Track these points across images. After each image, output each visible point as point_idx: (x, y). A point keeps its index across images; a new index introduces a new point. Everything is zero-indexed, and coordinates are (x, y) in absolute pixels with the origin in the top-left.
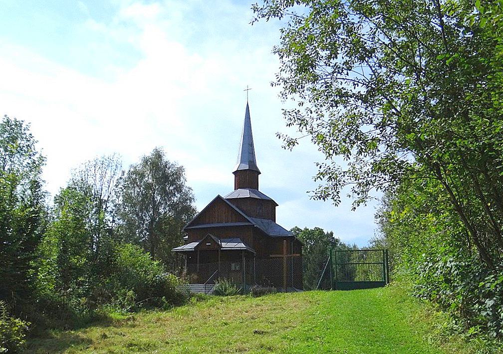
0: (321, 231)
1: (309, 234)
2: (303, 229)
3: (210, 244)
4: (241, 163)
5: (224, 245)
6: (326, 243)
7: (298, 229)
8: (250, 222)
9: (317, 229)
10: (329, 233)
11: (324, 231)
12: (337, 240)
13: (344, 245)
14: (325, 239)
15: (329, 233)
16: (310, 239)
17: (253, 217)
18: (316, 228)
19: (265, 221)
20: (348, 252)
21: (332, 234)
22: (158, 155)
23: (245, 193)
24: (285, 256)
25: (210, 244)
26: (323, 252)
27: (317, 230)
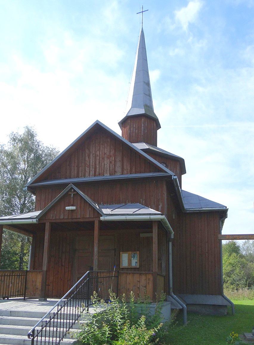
3: (74, 208)
22: (30, 135)
25: (74, 208)
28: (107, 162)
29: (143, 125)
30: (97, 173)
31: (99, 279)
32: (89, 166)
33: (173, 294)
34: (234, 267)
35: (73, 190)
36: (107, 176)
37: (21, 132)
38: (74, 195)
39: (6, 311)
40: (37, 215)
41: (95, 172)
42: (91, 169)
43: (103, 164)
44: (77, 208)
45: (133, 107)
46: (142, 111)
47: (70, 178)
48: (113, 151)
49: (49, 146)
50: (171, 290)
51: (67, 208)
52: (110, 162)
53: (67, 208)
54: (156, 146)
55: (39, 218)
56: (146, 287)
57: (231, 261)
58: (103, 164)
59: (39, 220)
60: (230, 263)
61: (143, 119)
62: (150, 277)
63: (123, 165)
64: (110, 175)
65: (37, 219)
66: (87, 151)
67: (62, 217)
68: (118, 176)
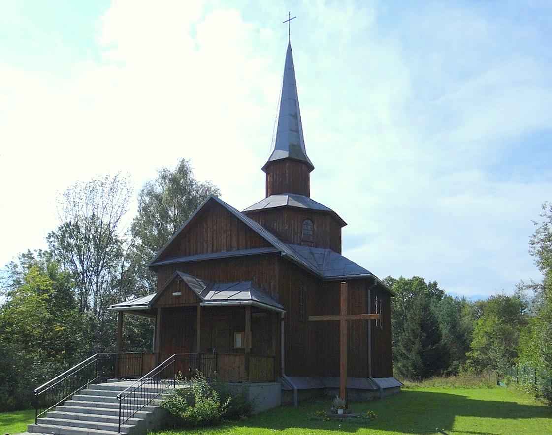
0: (421, 282)
1: (406, 285)
2: (398, 279)
3: (179, 294)
4: (275, 149)
5: (247, 295)
6: (429, 296)
7: (392, 280)
8: (270, 245)
9: (416, 278)
10: (432, 282)
11: (425, 281)
12: (442, 292)
13: (450, 298)
14: (426, 291)
15: (432, 282)
16: (407, 290)
17: (294, 244)
18: (415, 277)
19: (318, 251)
20: (457, 307)
21: (435, 284)
22: (183, 171)
23: (281, 201)
24: (343, 318)
25: (179, 294)
26: (426, 308)
27: (417, 280)
28: (223, 236)
29: (287, 171)
30: (215, 249)
31: (203, 360)
32: (207, 242)
33: (284, 375)
34: (492, 338)
35: (179, 277)
36: (224, 254)
37: (173, 169)
38: (179, 281)
39: (117, 387)
40: (150, 300)
41: (212, 249)
42: (209, 244)
43: (220, 239)
44: (182, 294)
45: (277, 147)
46: (284, 154)
47: (197, 253)
48: (230, 225)
49: (205, 184)
50: (283, 370)
51: (174, 294)
52: (227, 237)
53: (174, 294)
54: (307, 193)
55: (153, 303)
56: (239, 367)
57: (488, 329)
58: (220, 239)
59: (151, 306)
60: (485, 332)
61: (287, 164)
62: (243, 358)
63: (238, 239)
64: (227, 251)
65: (150, 305)
66: (205, 225)
67: (170, 303)
68: (235, 253)
